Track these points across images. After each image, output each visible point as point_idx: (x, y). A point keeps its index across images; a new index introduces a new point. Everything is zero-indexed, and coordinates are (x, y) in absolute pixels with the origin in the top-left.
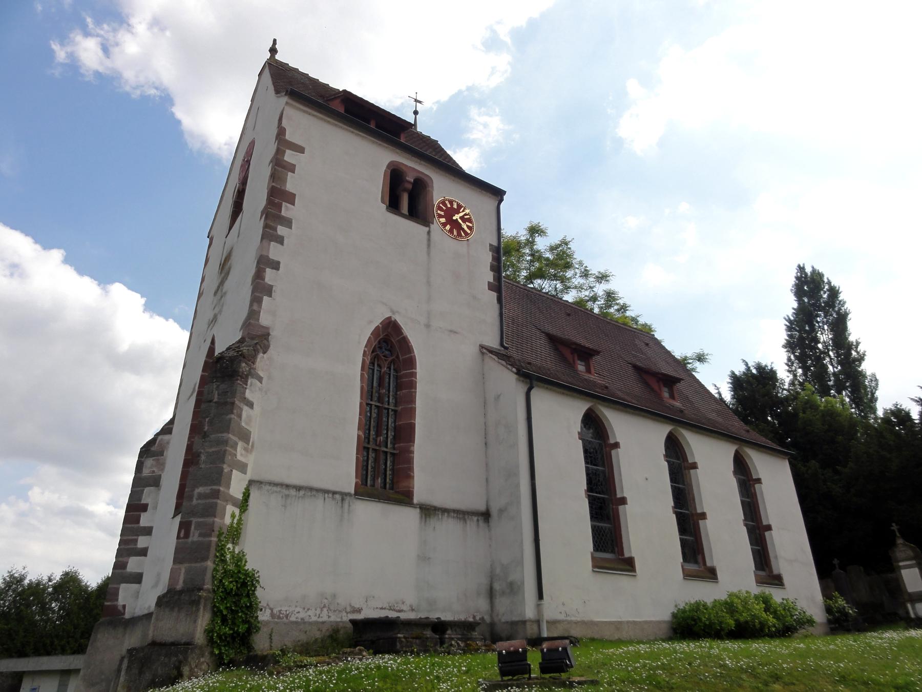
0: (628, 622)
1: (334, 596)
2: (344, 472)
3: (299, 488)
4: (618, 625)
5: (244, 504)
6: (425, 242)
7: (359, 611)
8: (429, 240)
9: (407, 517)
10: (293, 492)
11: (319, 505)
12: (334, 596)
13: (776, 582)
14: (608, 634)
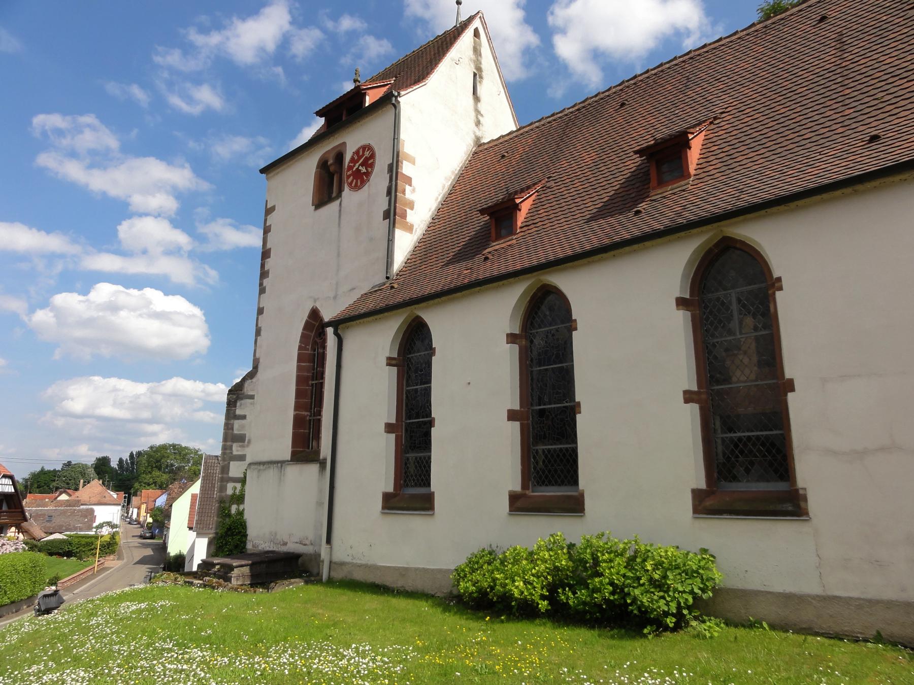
2: (284, 447)
5: (243, 481)
6: (337, 215)
7: (285, 544)
8: (340, 210)
10: (262, 467)
11: (272, 473)
12: (276, 534)
14: (389, 581)
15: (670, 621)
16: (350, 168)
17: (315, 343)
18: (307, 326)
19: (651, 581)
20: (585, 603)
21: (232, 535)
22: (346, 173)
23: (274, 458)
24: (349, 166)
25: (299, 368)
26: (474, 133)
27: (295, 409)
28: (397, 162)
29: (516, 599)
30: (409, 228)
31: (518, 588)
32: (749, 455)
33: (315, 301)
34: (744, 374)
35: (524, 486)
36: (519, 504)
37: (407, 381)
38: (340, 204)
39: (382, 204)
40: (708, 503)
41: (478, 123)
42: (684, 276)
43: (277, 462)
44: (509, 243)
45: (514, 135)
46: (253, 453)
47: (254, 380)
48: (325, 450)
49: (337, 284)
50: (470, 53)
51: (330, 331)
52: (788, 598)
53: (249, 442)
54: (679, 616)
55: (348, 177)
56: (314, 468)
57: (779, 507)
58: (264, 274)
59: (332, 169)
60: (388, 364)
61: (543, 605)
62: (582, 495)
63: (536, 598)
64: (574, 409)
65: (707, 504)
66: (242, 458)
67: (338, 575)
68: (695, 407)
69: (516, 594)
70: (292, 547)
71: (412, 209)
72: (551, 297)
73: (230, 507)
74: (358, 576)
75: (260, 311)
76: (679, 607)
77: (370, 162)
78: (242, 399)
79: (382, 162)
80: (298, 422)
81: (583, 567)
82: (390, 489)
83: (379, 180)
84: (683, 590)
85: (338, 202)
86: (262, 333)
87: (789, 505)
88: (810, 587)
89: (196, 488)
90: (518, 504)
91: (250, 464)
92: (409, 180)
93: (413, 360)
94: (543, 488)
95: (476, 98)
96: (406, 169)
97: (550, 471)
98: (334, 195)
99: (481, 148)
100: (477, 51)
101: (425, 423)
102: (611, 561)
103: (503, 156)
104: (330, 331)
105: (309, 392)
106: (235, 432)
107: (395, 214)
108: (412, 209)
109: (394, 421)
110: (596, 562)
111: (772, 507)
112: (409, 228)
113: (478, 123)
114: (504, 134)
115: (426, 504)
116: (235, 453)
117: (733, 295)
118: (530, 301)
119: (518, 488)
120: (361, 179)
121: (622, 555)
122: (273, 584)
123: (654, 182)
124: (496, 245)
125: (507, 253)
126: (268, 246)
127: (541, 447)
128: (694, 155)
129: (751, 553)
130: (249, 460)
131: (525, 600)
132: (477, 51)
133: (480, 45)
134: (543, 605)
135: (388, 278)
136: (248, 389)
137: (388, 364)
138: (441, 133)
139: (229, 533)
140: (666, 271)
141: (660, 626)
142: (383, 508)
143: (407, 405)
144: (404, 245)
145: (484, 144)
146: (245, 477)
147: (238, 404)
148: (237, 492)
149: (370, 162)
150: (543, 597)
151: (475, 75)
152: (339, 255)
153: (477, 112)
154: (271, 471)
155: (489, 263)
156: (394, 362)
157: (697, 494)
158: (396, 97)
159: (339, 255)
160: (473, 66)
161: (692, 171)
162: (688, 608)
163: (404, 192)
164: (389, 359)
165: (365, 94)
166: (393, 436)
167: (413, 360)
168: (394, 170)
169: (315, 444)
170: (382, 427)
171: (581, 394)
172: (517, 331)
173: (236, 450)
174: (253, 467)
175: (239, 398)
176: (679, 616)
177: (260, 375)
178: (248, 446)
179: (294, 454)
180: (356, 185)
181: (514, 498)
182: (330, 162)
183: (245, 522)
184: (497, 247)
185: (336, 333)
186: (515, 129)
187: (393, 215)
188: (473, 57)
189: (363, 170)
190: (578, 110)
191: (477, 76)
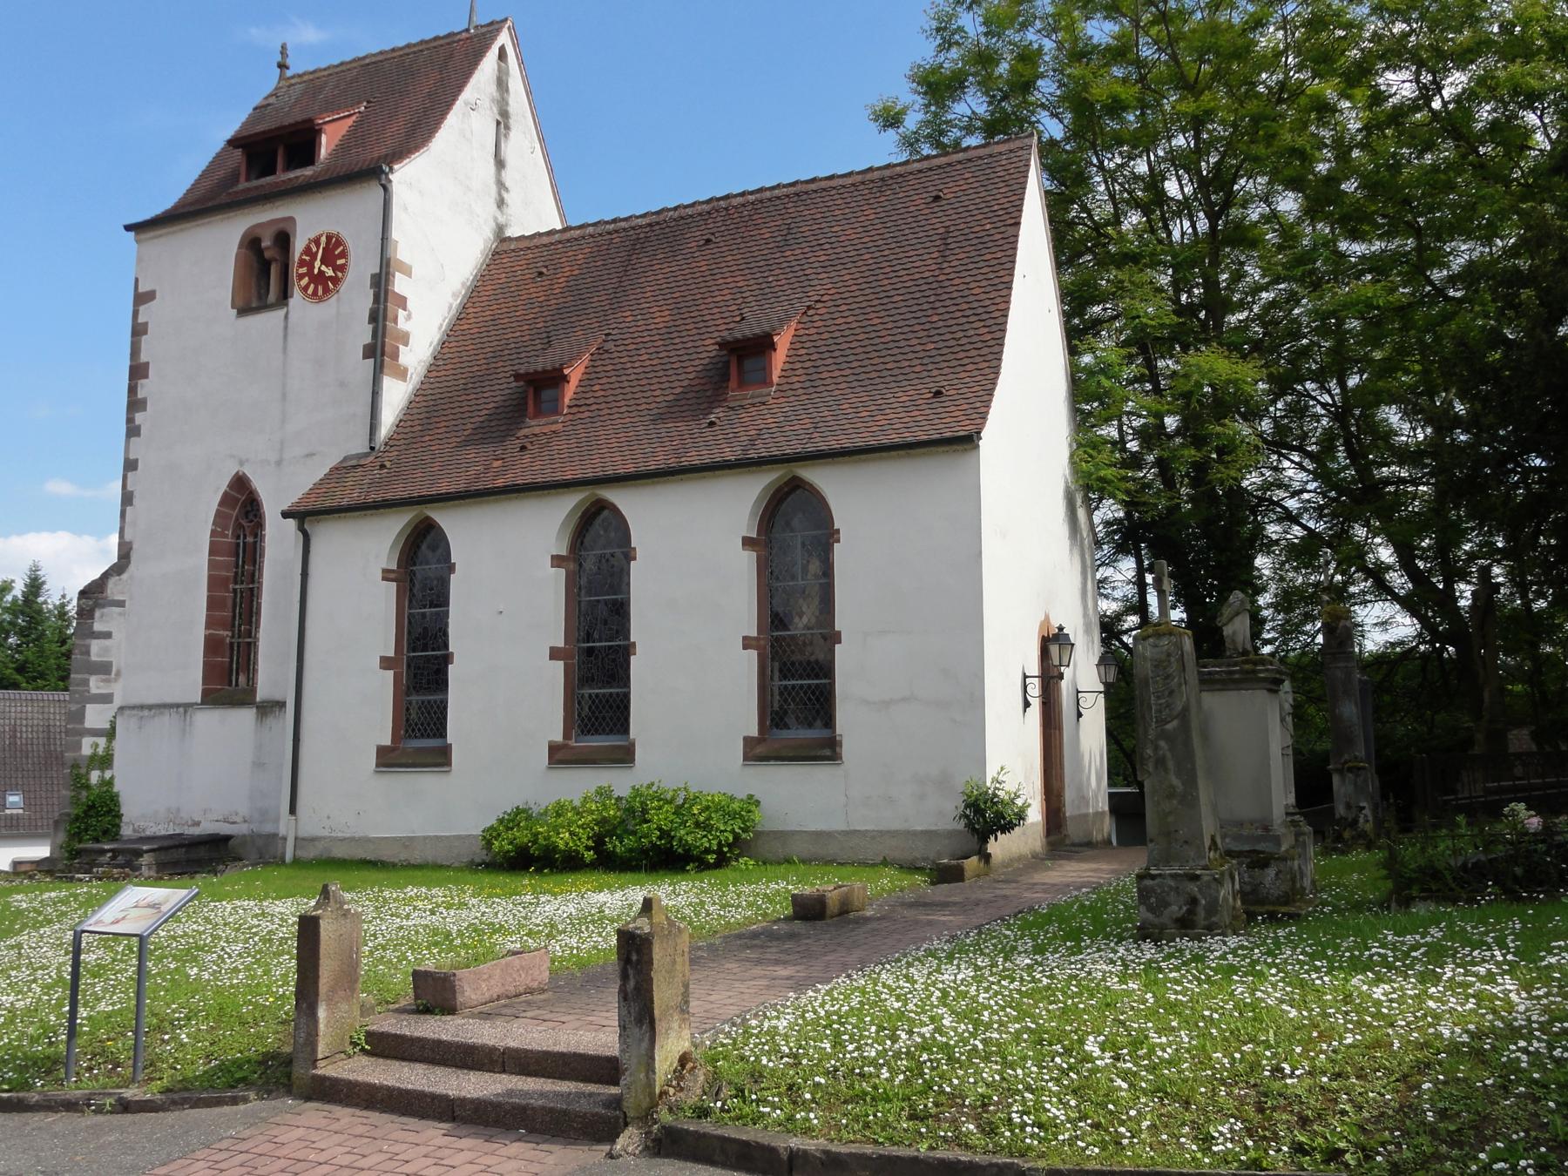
0: (425, 838)
1: (178, 810)
2: (191, 683)
3: (150, 707)
4: (407, 842)
5: (110, 734)
6: (281, 334)
7: (197, 824)
8: (286, 328)
9: (247, 715)
10: (146, 713)
11: (167, 721)
12: (178, 810)
13: (828, 752)
14: (386, 854)
15: (711, 858)
16: (302, 263)
17: (239, 526)
18: (226, 500)
19: (697, 824)
20: (631, 850)
21: (98, 815)
22: (295, 270)
23: (169, 700)
26: (495, 219)
27: (207, 627)
28: (388, 273)
29: (561, 851)
30: (402, 374)
31: (563, 840)
32: (798, 699)
33: (241, 463)
34: (802, 624)
35: (566, 735)
36: (559, 756)
38: (286, 317)
39: (363, 334)
40: (759, 750)
41: (501, 203)
42: (752, 514)
43: (178, 706)
44: (554, 427)
45: (557, 237)
47: (125, 576)
49: (282, 443)
50: (492, 89)
52: (818, 835)
53: (118, 674)
54: (719, 852)
55: (301, 277)
57: (819, 753)
58: (135, 404)
59: (267, 255)
60: (384, 579)
61: (589, 856)
62: (633, 745)
63: (581, 849)
64: (627, 650)
65: (757, 752)
66: (106, 699)
67: (309, 853)
68: (753, 654)
69: (561, 845)
70: (208, 827)
71: (406, 344)
72: (606, 513)
73: (88, 773)
74: (339, 852)
75: (130, 465)
76: (720, 844)
78: (103, 606)
79: (361, 267)
81: (636, 811)
82: (387, 741)
83: (355, 295)
84: (725, 830)
85: (281, 313)
87: (827, 750)
90: (559, 756)
91: (121, 709)
92: (402, 302)
93: (422, 576)
94: (589, 737)
95: (500, 164)
96: (400, 284)
98: (272, 297)
99: (505, 247)
100: (502, 84)
102: (660, 808)
103: (541, 274)
105: (230, 603)
106: (94, 658)
107: (383, 354)
108: (406, 344)
109: (391, 653)
110: (645, 811)
111: (813, 753)
112: (402, 374)
113: (501, 203)
114: (542, 230)
115: (441, 758)
116: (94, 690)
118: (581, 517)
120: (323, 286)
121: (670, 802)
122: (221, 867)
123: (733, 383)
124: (534, 426)
125: (553, 443)
126: (143, 358)
127: (587, 691)
128: (779, 358)
129: (794, 797)
131: (570, 851)
132: (502, 84)
133: (507, 74)
134: (589, 856)
135: (372, 448)
136: (114, 589)
137: (384, 579)
138: (451, 215)
139: (92, 813)
140: (734, 506)
141: (703, 866)
142: (378, 765)
144: (396, 396)
145: (510, 239)
146: (113, 728)
147: (97, 614)
148: (100, 751)
150: (588, 848)
151: (498, 123)
152: (284, 396)
153: (501, 185)
154: (166, 718)
155: (527, 458)
156: (392, 576)
157: (748, 741)
159: (284, 396)
160: (495, 110)
161: (775, 379)
162: (729, 845)
163: (395, 320)
164: (385, 571)
165: (319, 132)
166: (390, 673)
167: (422, 576)
168: (381, 283)
169: (242, 679)
170: (380, 575)
171: (638, 631)
172: (564, 553)
174: (127, 712)
175: (97, 605)
176: (719, 852)
179: (205, 693)
180: (315, 293)
181: (553, 749)
182: (266, 243)
183: (117, 795)
184: (537, 430)
186: (559, 227)
187: (380, 352)
188: (496, 94)
189: (329, 272)
190: (650, 225)
191: (503, 123)
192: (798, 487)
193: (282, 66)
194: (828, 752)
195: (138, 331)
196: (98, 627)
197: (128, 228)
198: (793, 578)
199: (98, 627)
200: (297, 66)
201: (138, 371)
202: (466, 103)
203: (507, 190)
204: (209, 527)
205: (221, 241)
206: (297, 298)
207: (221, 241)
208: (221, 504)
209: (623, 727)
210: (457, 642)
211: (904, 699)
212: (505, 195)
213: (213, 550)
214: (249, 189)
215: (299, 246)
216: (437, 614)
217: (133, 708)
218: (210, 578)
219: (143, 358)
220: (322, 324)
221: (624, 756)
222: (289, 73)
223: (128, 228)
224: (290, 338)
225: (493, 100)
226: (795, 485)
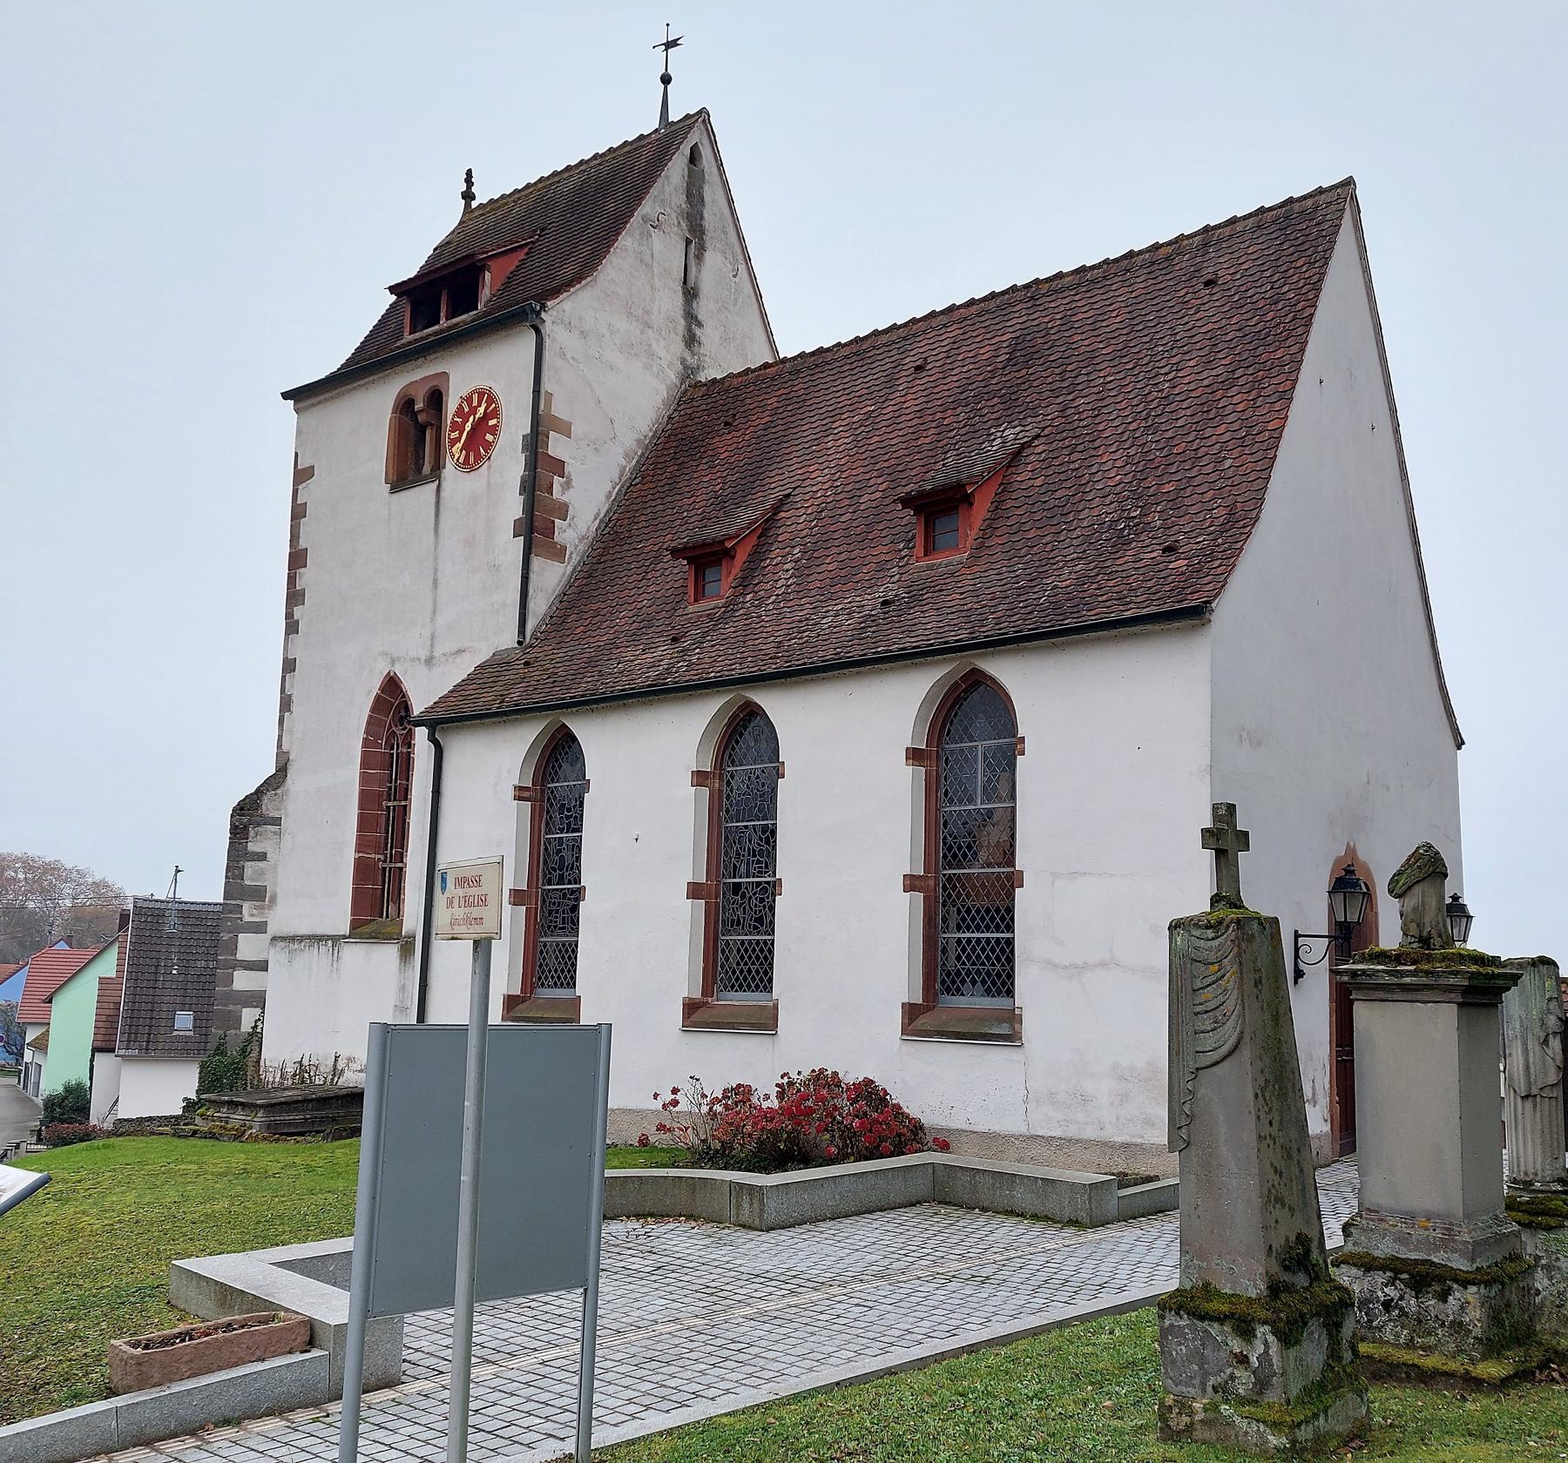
2: (338, 914)
8: (438, 503)
11: (325, 949)
18: (379, 705)
24: (453, 422)
25: (364, 779)
26: (683, 361)
27: (358, 850)
30: (559, 553)
33: (393, 663)
35: (707, 991)
36: (695, 1015)
37: (547, 824)
39: (513, 507)
41: (691, 340)
46: (282, 919)
48: (412, 918)
49: (433, 637)
50: (681, 199)
51: (421, 734)
53: (273, 900)
56: (390, 952)
58: (294, 597)
60: (518, 798)
65: (919, 1021)
66: (260, 928)
75: (289, 666)
77: (491, 423)
80: (363, 871)
86: (294, 707)
87: (1003, 1030)
88: (1013, 1125)
89: (108, 965)
91: (274, 939)
95: (690, 293)
97: (742, 972)
98: (426, 469)
101: (573, 892)
104: (421, 734)
112: (559, 553)
113: (691, 340)
116: (247, 918)
117: (980, 746)
118: (728, 725)
119: (697, 995)
126: (303, 544)
130: (273, 929)
136: (268, 807)
140: (895, 707)
143: (545, 862)
149: (491, 423)
151: (688, 242)
152: (435, 583)
153: (691, 318)
158: (538, 313)
164: (519, 789)
170: (511, 793)
173: (248, 912)
177: (294, 782)
178: (270, 907)
179: (355, 925)
181: (690, 1008)
185: (432, 739)
192: (978, 683)
193: (468, 196)
194: (1004, 1029)
195: (298, 512)
196: (252, 847)
197: (286, 396)
198: (971, 800)
199: (252, 847)
200: (482, 196)
201: (297, 559)
202: (645, 219)
203: (700, 324)
204: (362, 735)
205: (375, 407)
206: (449, 469)
207: (375, 407)
208: (373, 710)
209: (766, 984)
210: (590, 875)
211: (1102, 964)
212: (698, 331)
213: (365, 764)
214: (416, 341)
215: (451, 405)
216: (574, 839)
217: (283, 939)
218: (362, 792)
219: (303, 544)
220: (487, 493)
221: (765, 1022)
222: (474, 204)
223: (286, 396)
224: (442, 517)
225: (681, 214)
226: (977, 681)
